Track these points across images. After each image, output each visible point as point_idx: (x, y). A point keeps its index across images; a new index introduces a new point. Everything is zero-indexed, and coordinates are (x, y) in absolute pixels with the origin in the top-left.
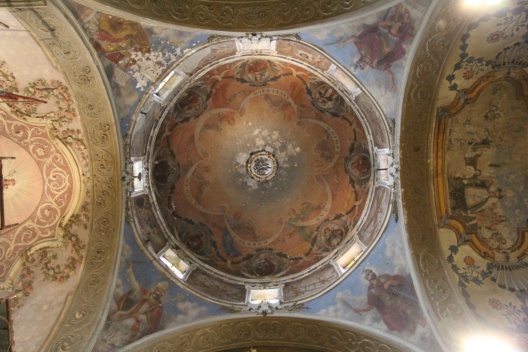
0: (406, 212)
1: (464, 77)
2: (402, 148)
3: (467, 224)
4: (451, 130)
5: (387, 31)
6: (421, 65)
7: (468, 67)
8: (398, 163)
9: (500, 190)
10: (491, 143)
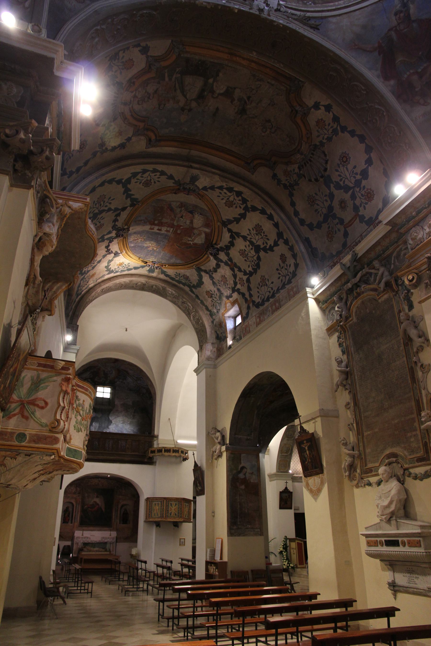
0: (209, 7)
1: (322, 119)
2: (285, 28)
3: (166, 71)
4: (273, 85)
5: (420, 70)
6: (365, 92)
7: (329, 127)
8: (269, 15)
9: (190, 110)
10: (240, 116)
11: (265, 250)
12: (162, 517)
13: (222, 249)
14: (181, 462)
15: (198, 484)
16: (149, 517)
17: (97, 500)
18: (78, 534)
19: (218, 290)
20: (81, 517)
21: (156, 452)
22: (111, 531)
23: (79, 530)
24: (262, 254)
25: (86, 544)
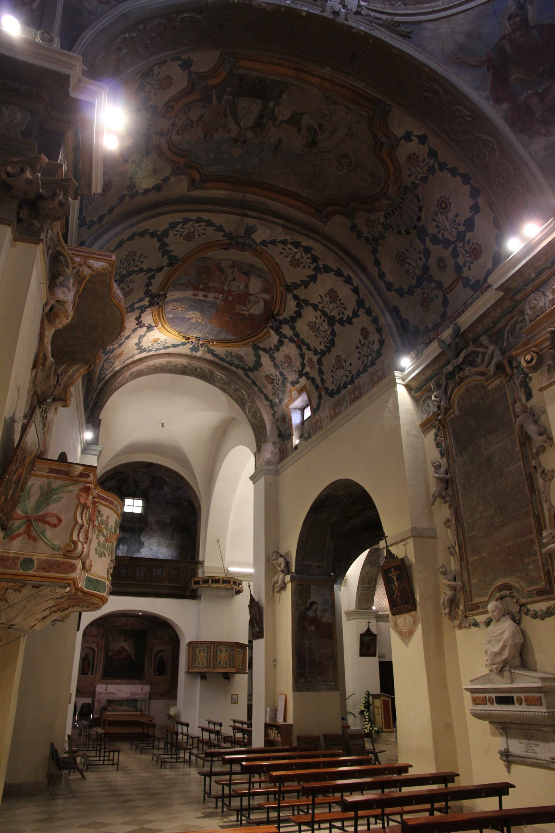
0: (269, 9)
1: (414, 154)
2: (367, 36)
3: (214, 91)
4: (351, 109)
5: (540, 91)
6: (470, 119)
7: (424, 164)
8: (346, 19)
9: (245, 142)
10: (309, 149)
11: (341, 322)
12: (208, 666)
13: (285, 321)
14: (233, 596)
15: (255, 625)
16: (192, 667)
17: (125, 645)
18: (100, 688)
19: (281, 374)
20: (105, 667)
21: (201, 583)
22: (142, 684)
23: (102, 683)
24: (337, 327)
25: (110, 702)
